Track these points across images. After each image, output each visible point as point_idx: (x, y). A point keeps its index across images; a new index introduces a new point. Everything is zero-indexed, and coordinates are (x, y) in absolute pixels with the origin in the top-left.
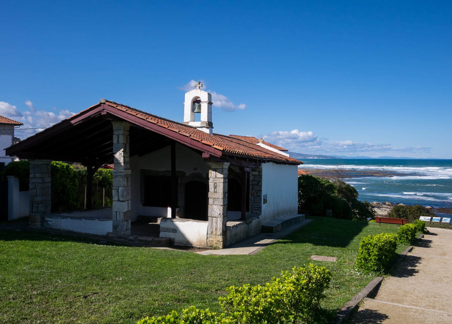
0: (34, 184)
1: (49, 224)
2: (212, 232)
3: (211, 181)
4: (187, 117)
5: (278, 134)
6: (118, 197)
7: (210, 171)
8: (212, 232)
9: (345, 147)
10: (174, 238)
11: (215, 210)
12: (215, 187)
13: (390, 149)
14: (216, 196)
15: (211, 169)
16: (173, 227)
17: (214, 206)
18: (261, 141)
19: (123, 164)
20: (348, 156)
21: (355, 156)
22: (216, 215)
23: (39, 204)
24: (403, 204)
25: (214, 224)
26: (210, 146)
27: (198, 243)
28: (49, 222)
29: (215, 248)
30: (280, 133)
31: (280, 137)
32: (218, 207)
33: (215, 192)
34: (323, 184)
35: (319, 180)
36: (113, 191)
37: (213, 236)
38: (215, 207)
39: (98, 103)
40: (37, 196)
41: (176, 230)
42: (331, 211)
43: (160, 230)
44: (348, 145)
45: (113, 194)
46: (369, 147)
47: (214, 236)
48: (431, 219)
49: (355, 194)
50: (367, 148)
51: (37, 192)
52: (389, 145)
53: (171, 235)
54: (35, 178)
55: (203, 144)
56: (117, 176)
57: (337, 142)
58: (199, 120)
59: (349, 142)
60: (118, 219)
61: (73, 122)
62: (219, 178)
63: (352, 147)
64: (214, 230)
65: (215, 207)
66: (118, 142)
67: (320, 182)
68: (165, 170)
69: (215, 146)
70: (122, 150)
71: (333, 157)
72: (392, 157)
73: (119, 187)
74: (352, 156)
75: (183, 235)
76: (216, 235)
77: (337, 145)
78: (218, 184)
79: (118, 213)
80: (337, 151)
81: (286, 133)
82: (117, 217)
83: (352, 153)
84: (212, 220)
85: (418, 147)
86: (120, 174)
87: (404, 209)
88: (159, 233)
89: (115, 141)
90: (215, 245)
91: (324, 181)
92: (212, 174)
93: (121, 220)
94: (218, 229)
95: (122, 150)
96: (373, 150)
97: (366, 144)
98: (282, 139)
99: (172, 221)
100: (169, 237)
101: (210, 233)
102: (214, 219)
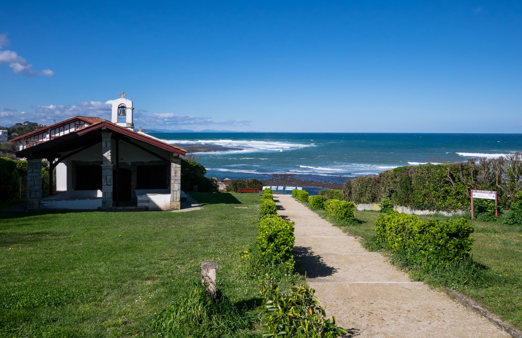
0: (32, 178)
1: (44, 206)
2: (174, 200)
3: (172, 169)
4: (114, 120)
5: (89, 105)
6: (107, 183)
7: (172, 163)
8: (174, 200)
9: (166, 120)
10: (148, 206)
11: (176, 187)
12: (176, 173)
13: (211, 122)
14: (176, 178)
15: (173, 162)
16: (147, 199)
17: (175, 184)
18: (140, 130)
19: (110, 161)
20: (170, 129)
21: (177, 130)
22: (176, 189)
23: (37, 191)
24: (229, 178)
25: (175, 195)
26: (179, 149)
27: (165, 208)
28: (44, 205)
29: (176, 209)
30: (92, 103)
31: (91, 108)
32: (178, 185)
33: (175, 176)
34: (192, 165)
35: (188, 162)
36: (103, 179)
37: (174, 202)
38: (175, 185)
39: (101, 122)
40: (35, 186)
41: (149, 201)
42: (197, 187)
43: (138, 202)
44: (168, 118)
45: (103, 181)
46: (190, 119)
47: (175, 202)
48: (277, 188)
49: (204, 172)
50: (188, 121)
51: (35, 183)
52: (211, 118)
53: (146, 204)
54: (33, 172)
55: (175, 148)
56: (106, 169)
57: (157, 115)
58: (125, 122)
59: (171, 115)
60: (107, 197)
61: (79, 134)
62: (178, 167)
63: (174, 120)
64: (175, 199)
65: (175, 185)
66: (106, 146)
67: (189, 163)
68: (95, 160)
69: (182, 150)
70: (110, 151)
71: (153, 131)
72: (214, 130)
73: (107, 176)
74: (174, 130)
75: (153, 203)
76: (176, 201)
77: (157, 118)
78: (177, 171)
79: (107, 194)
80: (157, 124)
81: (99, 103)
82: (105, 196)
83: (173, 127)
84: (174, 193)
85: (239, 120)
86: (108, 167)
87: (240, 183)
88: (137, 203)
89: (104, 145)
90: (175, 208)
91: (192, 163)
92: (173, 165)
93: (109, 198)
94: (178, 198)
95: (110, 151)
96: (195, 123)
97: (187, 117)
98: (93, 110)
99: (147, 196)
100: (145, 206)
101: (172, 201)
102: (175, 192)
